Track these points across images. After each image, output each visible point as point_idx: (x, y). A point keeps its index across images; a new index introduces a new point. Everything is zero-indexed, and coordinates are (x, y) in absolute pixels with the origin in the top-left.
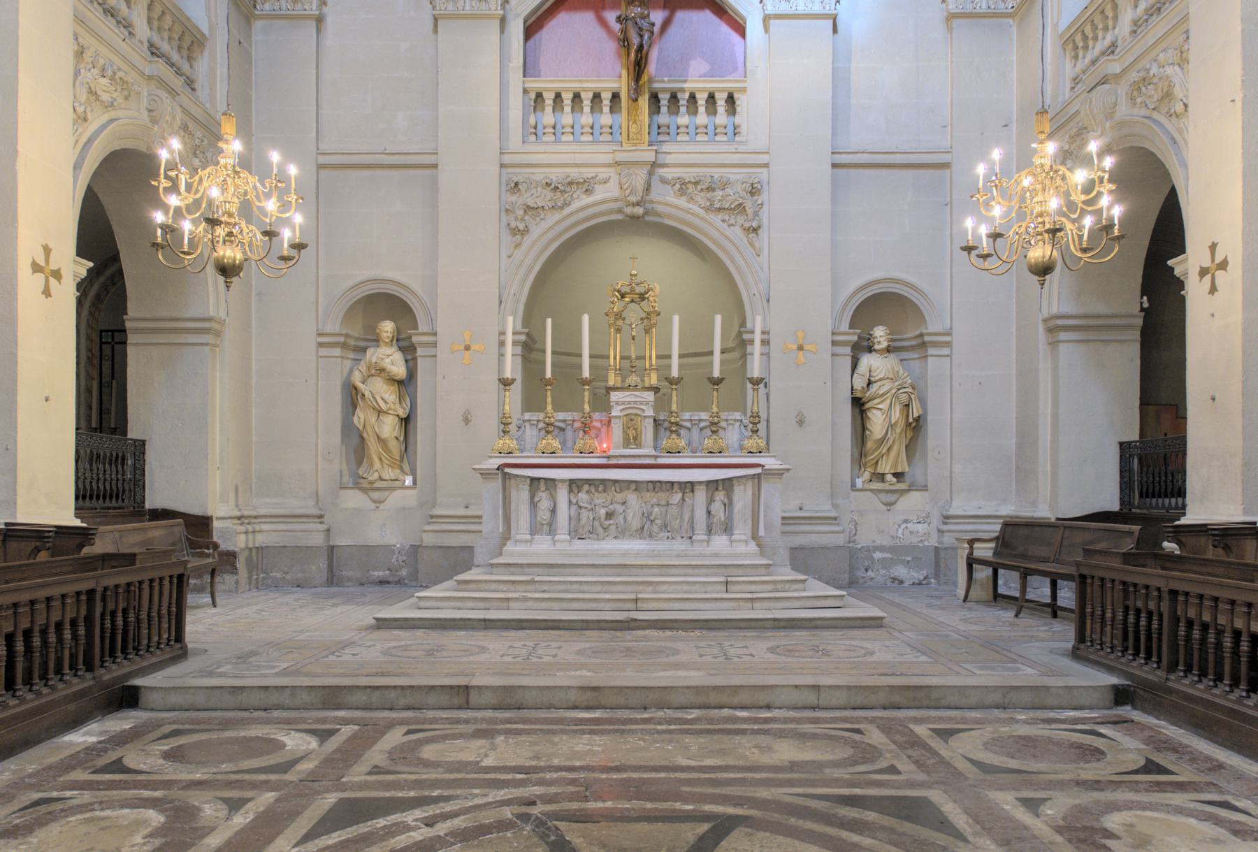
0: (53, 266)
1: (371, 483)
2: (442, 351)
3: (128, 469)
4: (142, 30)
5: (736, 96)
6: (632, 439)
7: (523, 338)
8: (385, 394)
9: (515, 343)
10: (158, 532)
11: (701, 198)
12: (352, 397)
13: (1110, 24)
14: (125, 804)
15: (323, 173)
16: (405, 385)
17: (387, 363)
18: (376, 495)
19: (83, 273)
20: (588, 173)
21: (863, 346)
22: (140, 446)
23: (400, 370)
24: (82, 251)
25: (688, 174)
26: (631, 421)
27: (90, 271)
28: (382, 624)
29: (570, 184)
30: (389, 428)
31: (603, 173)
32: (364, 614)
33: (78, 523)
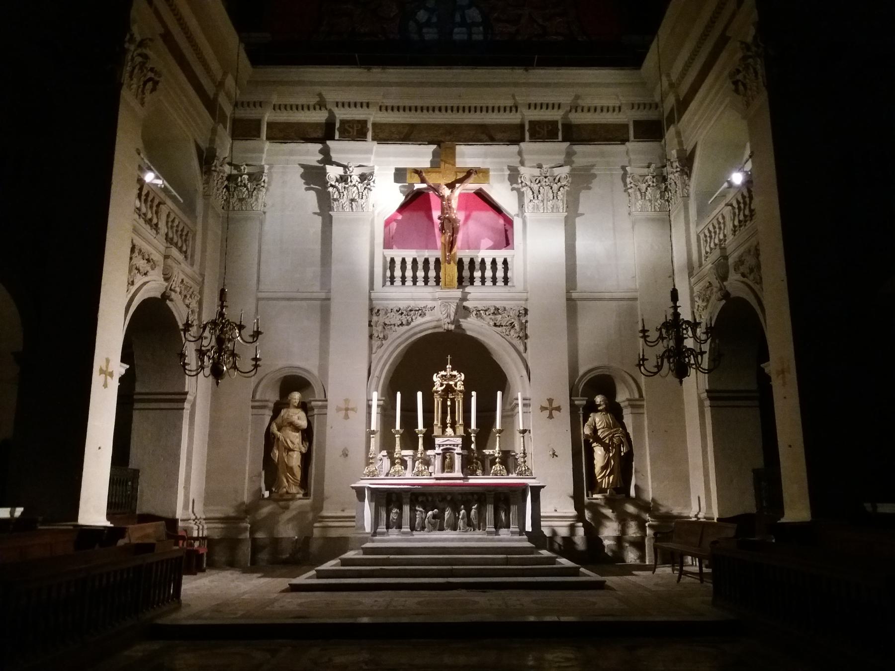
0: (110, 370)
1: (282, 495)
2: (331, 411)
3: (129, 488)
4: (163, 229)
5: (508, 260)
6: (447, 465)
7: (382, 402)
8: (294, 438)
9: (378, 406)
10: (150, 529)
11: (487, 318)
12: (270, 440)
13: (722, 226)
14: (742, 391)
15: (323, 398)
16: (307, 434)
17: (295, 419)
18: (281, 503)
19: (123, 372)
20: (421, 304)
21: (592, 408)
22: (136, 473)
23: (303, 423)
24: (124, 360)
25: (480, 305)
26: (447, 451)
27: (127, 370)
28: (295, 588)
29: (411, 310)
30: (295, 460)
31: (430, 304)
32: (284, 583)
33: (108, 524)
